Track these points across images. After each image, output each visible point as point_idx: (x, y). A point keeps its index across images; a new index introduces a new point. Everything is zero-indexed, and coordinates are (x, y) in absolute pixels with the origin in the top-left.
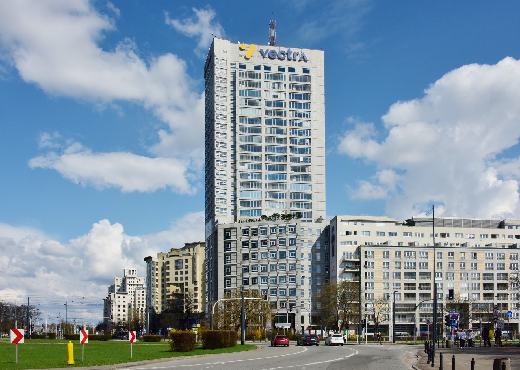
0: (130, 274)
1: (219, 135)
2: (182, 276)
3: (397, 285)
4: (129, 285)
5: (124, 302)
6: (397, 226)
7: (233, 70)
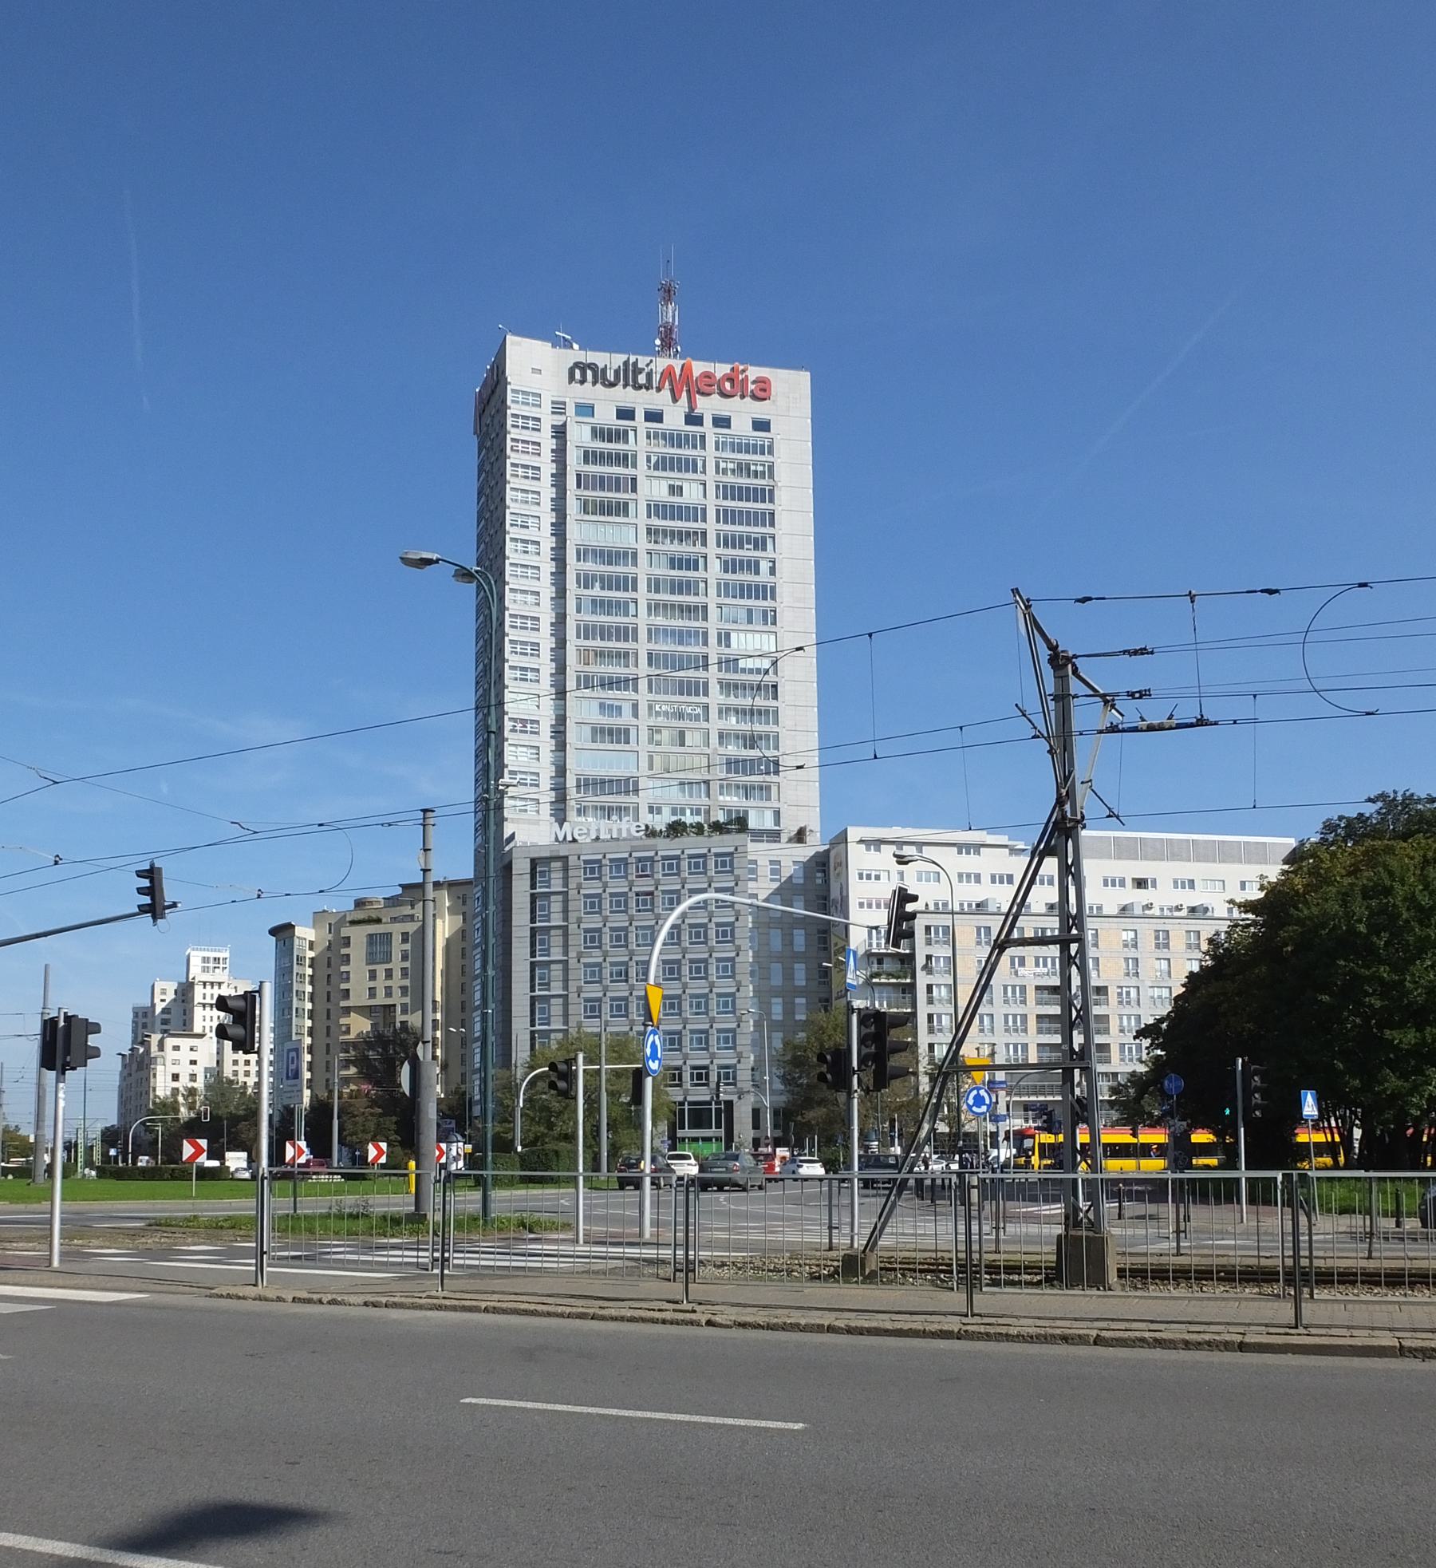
0: (205, 970)
1: (519, 596)
2: (389, 983)
3: (1015, 1021)
4: (204, 1005)
5: (193, 1062)
6: (1014, 858)
7: (559, 420)
